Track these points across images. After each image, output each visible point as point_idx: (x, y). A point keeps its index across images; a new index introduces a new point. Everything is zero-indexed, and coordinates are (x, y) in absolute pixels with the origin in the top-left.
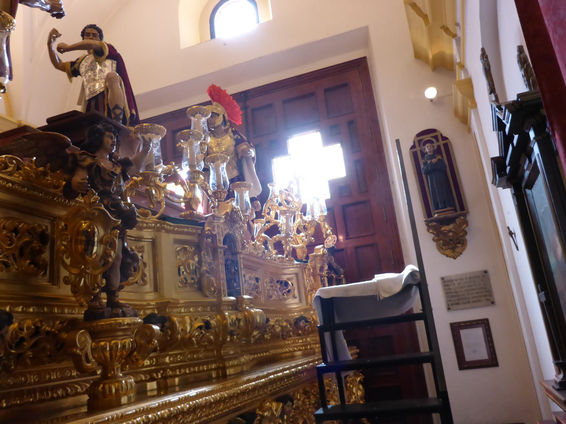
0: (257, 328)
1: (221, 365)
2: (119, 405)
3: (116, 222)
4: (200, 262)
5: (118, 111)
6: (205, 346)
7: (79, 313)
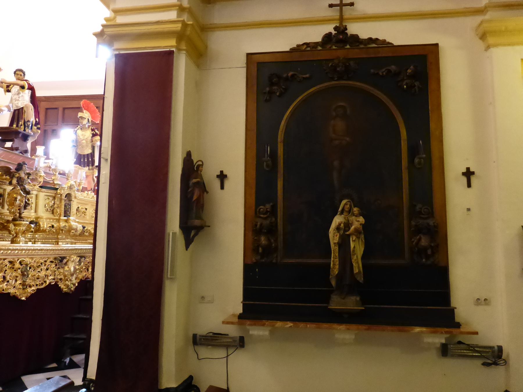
0: (73, 229)
1: (57, 241)
2: (19, 243)
3: (24, 195)
4: (54, 204)
5: (29, 123)
6: (51, 233)
7: (10, 218)
